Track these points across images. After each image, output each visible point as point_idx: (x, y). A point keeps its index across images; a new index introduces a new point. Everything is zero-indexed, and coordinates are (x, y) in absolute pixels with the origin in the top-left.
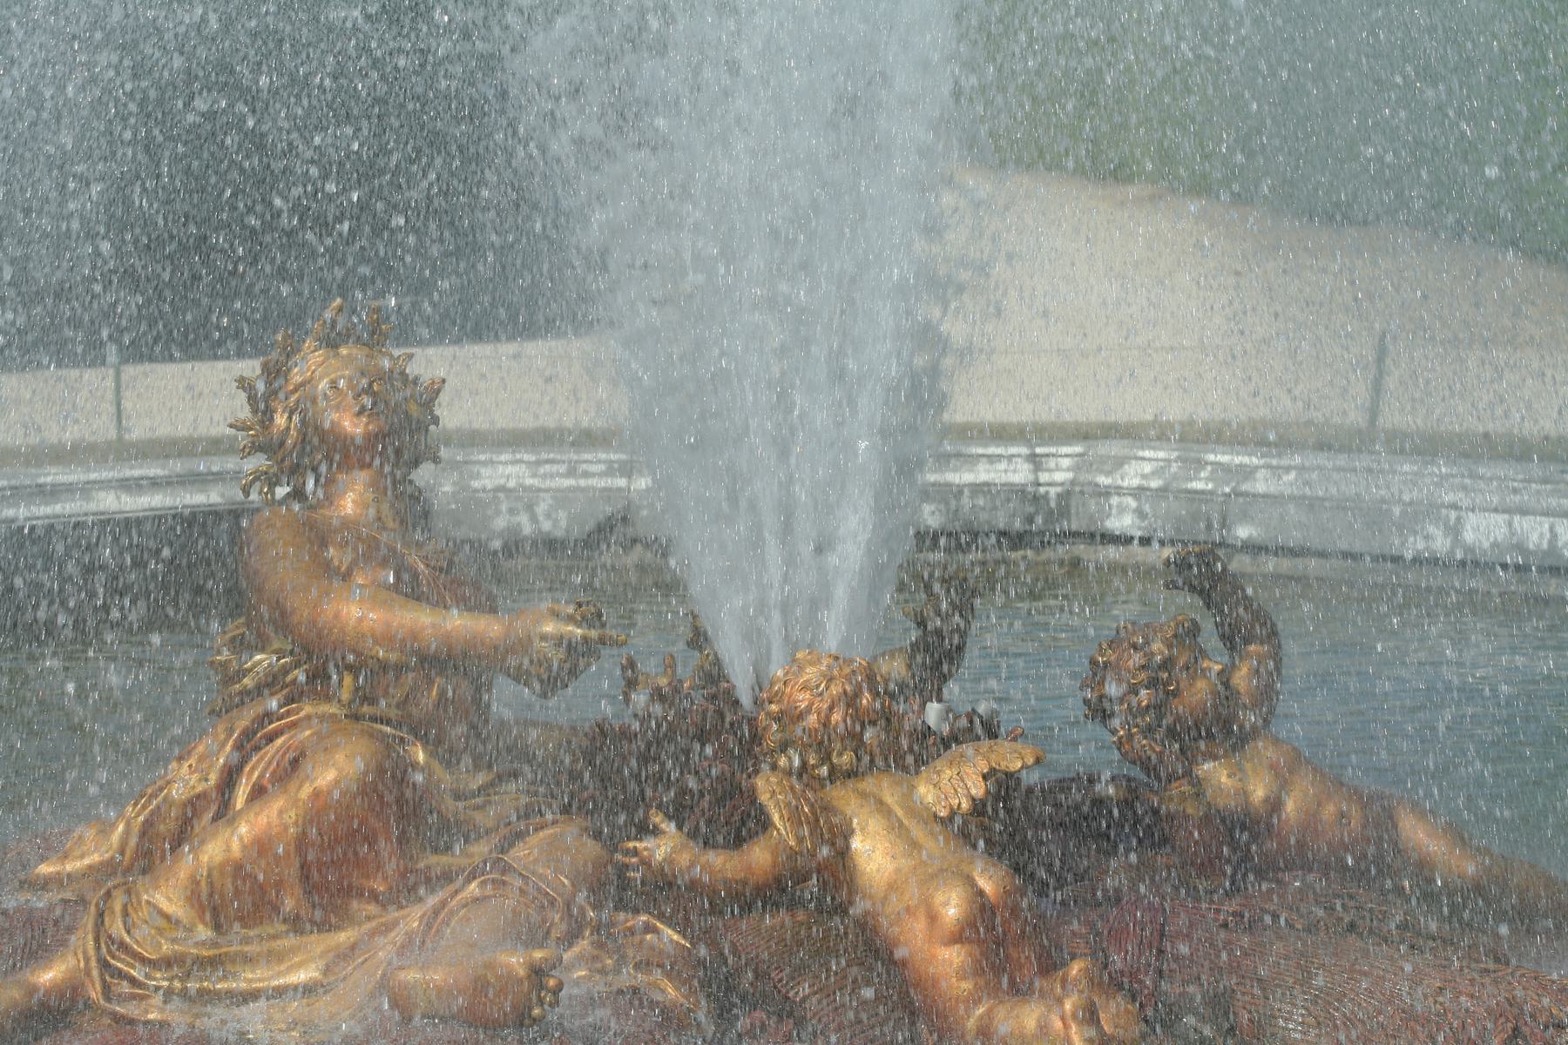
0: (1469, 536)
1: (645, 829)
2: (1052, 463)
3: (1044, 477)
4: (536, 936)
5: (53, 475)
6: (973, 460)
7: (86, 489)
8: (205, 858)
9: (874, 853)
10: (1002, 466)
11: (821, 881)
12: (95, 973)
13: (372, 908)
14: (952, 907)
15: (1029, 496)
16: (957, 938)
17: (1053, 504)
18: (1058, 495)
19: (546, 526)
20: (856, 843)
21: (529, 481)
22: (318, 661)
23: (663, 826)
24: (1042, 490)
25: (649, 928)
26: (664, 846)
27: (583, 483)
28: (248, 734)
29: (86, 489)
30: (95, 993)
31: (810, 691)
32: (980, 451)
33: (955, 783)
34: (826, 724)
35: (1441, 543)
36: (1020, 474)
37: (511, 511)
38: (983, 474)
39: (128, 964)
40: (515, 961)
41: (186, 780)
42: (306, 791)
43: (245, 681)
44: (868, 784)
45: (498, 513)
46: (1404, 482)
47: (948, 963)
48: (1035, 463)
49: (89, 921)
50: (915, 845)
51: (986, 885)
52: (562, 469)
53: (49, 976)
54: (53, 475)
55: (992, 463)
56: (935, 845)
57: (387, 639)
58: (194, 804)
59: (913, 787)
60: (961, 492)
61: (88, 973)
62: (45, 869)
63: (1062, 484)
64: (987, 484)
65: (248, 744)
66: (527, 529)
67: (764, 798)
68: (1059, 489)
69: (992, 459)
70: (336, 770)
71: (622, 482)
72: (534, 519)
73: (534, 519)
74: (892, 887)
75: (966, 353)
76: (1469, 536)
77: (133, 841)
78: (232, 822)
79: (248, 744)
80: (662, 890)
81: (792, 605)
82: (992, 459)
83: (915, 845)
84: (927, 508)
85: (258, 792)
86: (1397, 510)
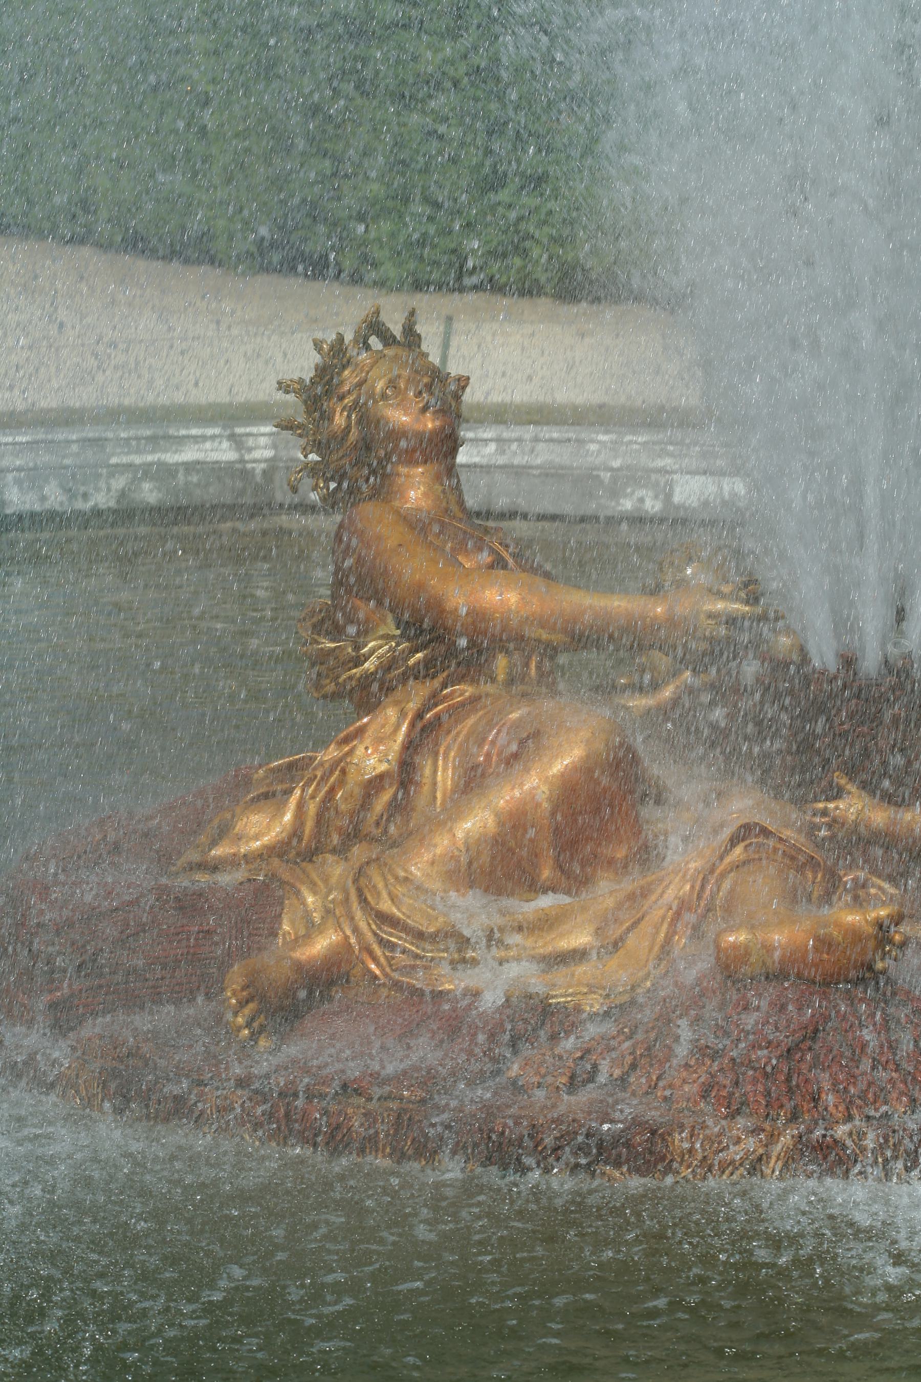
0: (677, 499)
2: (250, 442)
6: (181, 441)
8: (460, 835)
10: (208, 445)
15: (238, 472)
17: (258, 478)
18: (264, 472)
23: (849, 787)
24: (249, 466)
32: (183, 432)
35: (652, 506)
36: (225, 453)
38: (189, 454)
39: (400, 938)
43: (366, 665)
46: (600, 449)
48: (236, 442)
55: (197, 442)
60: (177, 471)
62: (217, 852)
63: (266, 461)
64: (198, 462)
68: (263, 466)
69: (197, 439)
76: (677, 499)
82: (197, 439)
84: (146, 486)
86: (606, 476)
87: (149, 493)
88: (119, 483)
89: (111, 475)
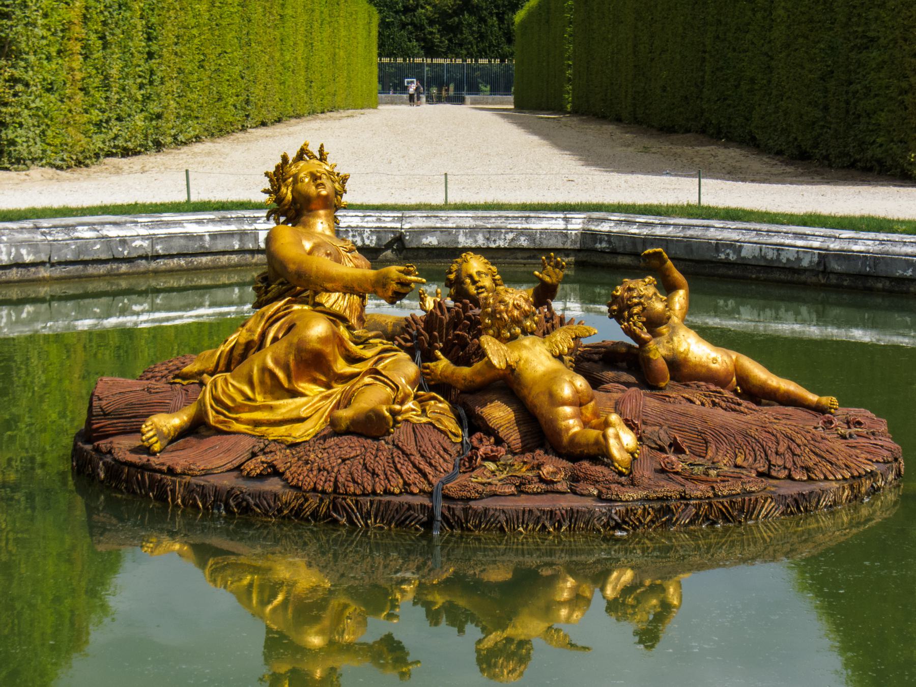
1: (437, 359)
2: (574, 221)
3: (570, 227)
10: (554, 222)
19: (367, 242)
21: (360, 224)
27: (383, 225)
37: (354, 236)
52: (374, 219)
54: (167, 217)
71: (398, 225)
72: (363, 241)
73: (363, 241)
84: (522, 238)
87: (523, 242)
88: (510, 236)
89: (507, 233)
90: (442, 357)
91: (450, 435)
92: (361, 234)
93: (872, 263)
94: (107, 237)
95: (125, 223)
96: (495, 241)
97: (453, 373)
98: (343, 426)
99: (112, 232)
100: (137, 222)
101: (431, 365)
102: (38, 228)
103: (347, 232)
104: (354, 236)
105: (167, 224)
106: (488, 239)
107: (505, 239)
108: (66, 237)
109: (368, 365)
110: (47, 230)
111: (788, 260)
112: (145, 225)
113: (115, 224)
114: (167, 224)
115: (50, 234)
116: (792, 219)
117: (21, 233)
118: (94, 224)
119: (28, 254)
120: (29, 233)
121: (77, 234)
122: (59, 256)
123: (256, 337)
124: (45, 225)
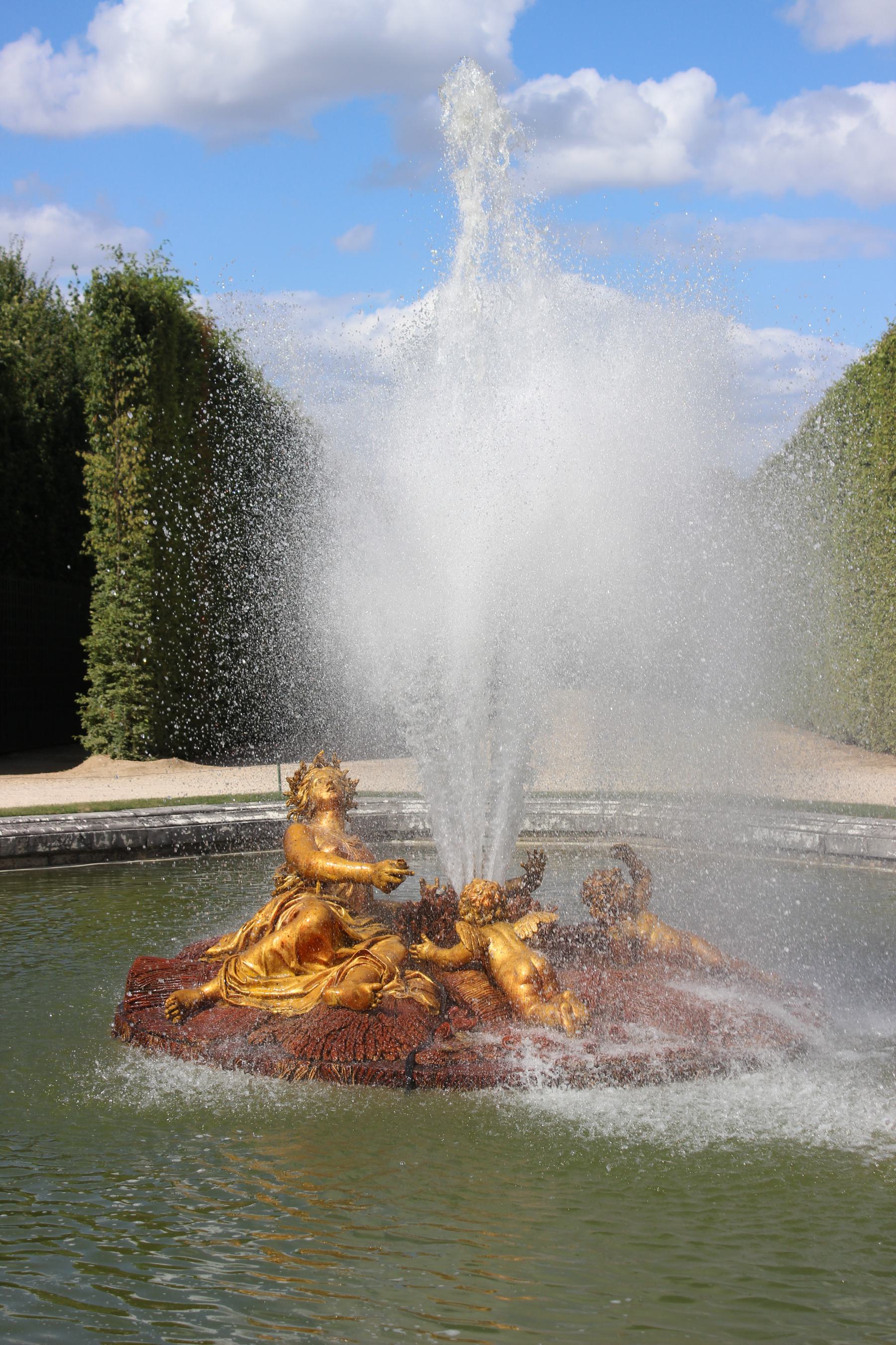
1: (420, 942)
4: (376, 978)
5: (252, 806)
7: (263, 811)
9: (498, 951)
11: (480, 962)
12: (224, 988)
13: (322, 967)
14: (524, 971)
16: (527, 981)
20: (491, 947)
22: (310, 880)
25: (418, 976)
26: (426, 948)
28: (282, 905)
29: (263, 811)
30: (223, 994)
31: (479, 893)
33: (528, 926)
34: (482, 905)
37: (416, 821)
38: (585, 810)
40: (367, 988)
41: (259, 920)
42: (299, 926)
44: (495, 926)
45: (411, 822)
47: (522, 991)
49: (222, 970)
50: (511, 947)
51: (537, 964)
53: (208, 989)
54: (252, 806)
56: (518, 947)
57: (334, 872)
58: (262, 930)
59: (513, 928)
61: (221, 988)
65: (282, 908)
66: (421, 827)
67: (458, 930)
69: (588, 805)
70: (311, 919)
72: (424, 824)
74: (504, 963)
75: (118, 883)
77: (242, 941)
78: (275, 934)
79: (282, 908)
80: (428, 965)
81: (468, 865)
82: (588, 805)
83: (511, 947)
85: (284, 924)
87: (565, 826)
89: (551, 818)
90: (426, 940)
91: (20, 1154)
92: (422, 820)
93: (865, 846)
94: (198, 823)
95: (215, 811)
96: (539, 825)
97: (435, 955)
98: (334, 1002)
99: (203, 819)
100: (224, 811)
101: (419, 946)
102: (137, 816)
103: (410, 818)
104: (416, 821)
105: (252, 811)
106: (533, 823)
107: (549, 823)
108: (162, 824)
109: (360, 947)
110: (145, 819)
111: (793, 842)
112: (231, 813)
113: (203, 812)
114: (252, 811)
115: (147, 822)
116: (130, 805)
117: (122, 821)
118: (187, 813)
119: (127, 840)
120: (129, 820)
121: (171, 822)
122: (154, 841)
123: (268, 922)
124: (144, 814)
